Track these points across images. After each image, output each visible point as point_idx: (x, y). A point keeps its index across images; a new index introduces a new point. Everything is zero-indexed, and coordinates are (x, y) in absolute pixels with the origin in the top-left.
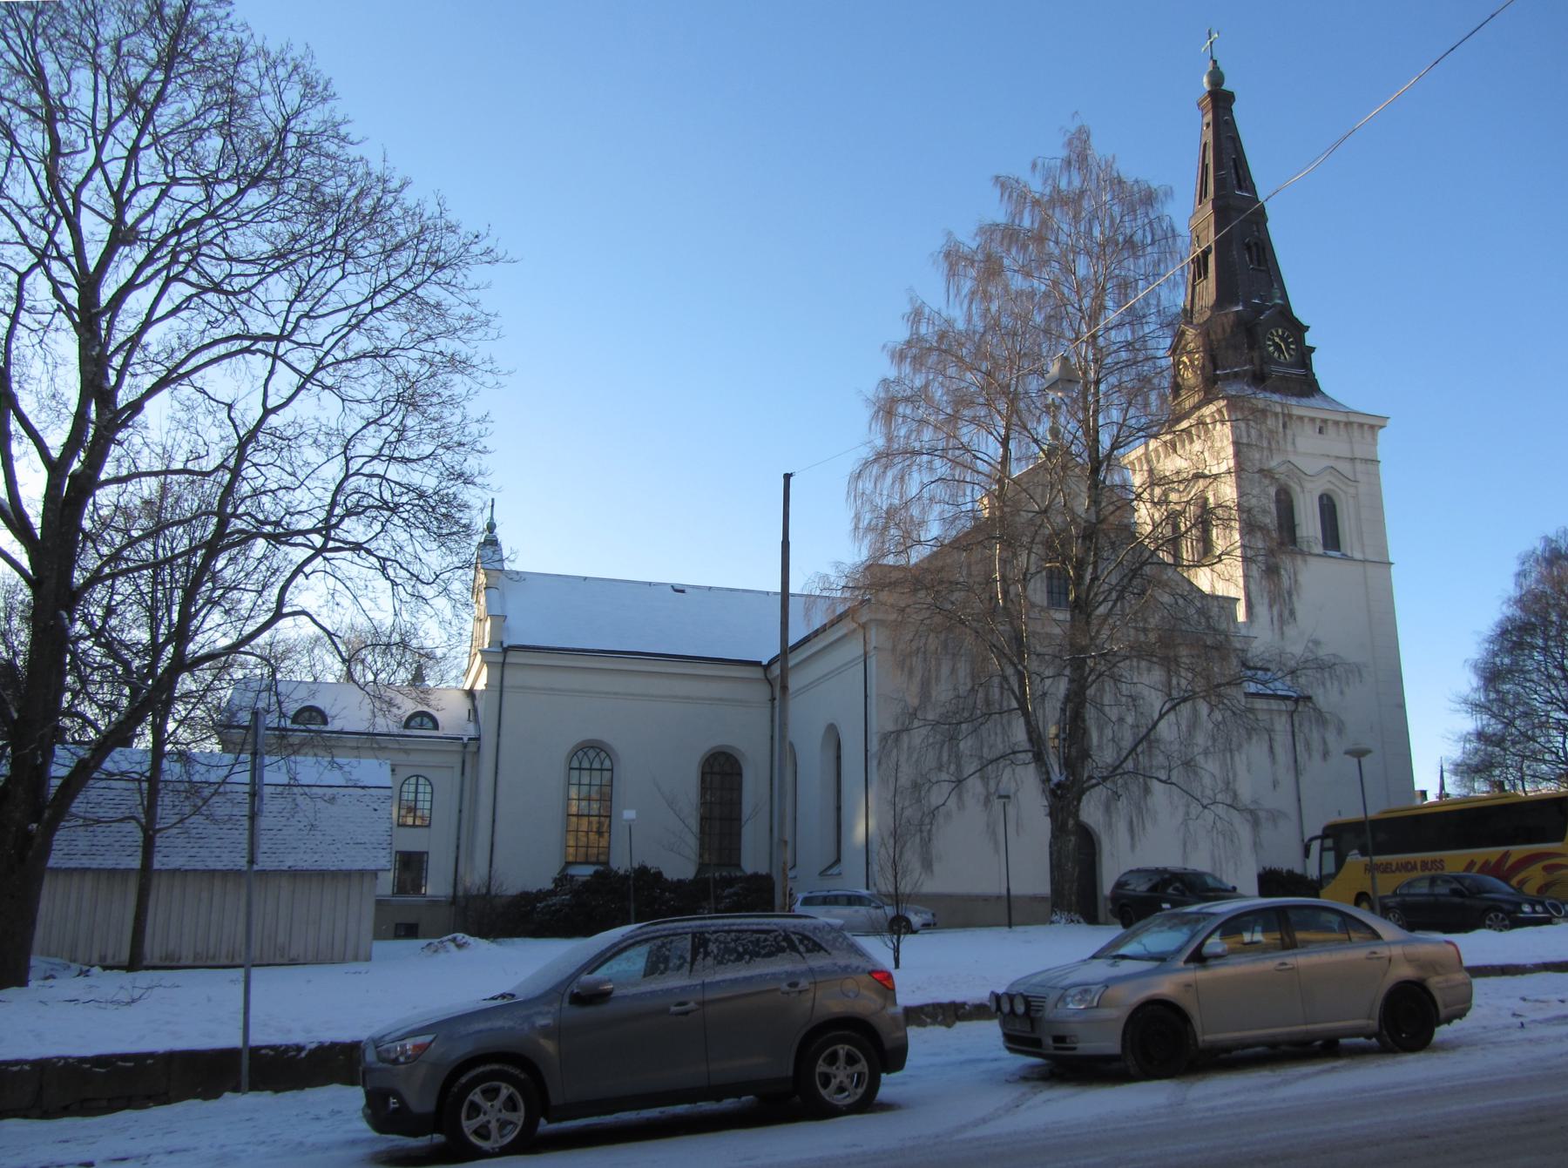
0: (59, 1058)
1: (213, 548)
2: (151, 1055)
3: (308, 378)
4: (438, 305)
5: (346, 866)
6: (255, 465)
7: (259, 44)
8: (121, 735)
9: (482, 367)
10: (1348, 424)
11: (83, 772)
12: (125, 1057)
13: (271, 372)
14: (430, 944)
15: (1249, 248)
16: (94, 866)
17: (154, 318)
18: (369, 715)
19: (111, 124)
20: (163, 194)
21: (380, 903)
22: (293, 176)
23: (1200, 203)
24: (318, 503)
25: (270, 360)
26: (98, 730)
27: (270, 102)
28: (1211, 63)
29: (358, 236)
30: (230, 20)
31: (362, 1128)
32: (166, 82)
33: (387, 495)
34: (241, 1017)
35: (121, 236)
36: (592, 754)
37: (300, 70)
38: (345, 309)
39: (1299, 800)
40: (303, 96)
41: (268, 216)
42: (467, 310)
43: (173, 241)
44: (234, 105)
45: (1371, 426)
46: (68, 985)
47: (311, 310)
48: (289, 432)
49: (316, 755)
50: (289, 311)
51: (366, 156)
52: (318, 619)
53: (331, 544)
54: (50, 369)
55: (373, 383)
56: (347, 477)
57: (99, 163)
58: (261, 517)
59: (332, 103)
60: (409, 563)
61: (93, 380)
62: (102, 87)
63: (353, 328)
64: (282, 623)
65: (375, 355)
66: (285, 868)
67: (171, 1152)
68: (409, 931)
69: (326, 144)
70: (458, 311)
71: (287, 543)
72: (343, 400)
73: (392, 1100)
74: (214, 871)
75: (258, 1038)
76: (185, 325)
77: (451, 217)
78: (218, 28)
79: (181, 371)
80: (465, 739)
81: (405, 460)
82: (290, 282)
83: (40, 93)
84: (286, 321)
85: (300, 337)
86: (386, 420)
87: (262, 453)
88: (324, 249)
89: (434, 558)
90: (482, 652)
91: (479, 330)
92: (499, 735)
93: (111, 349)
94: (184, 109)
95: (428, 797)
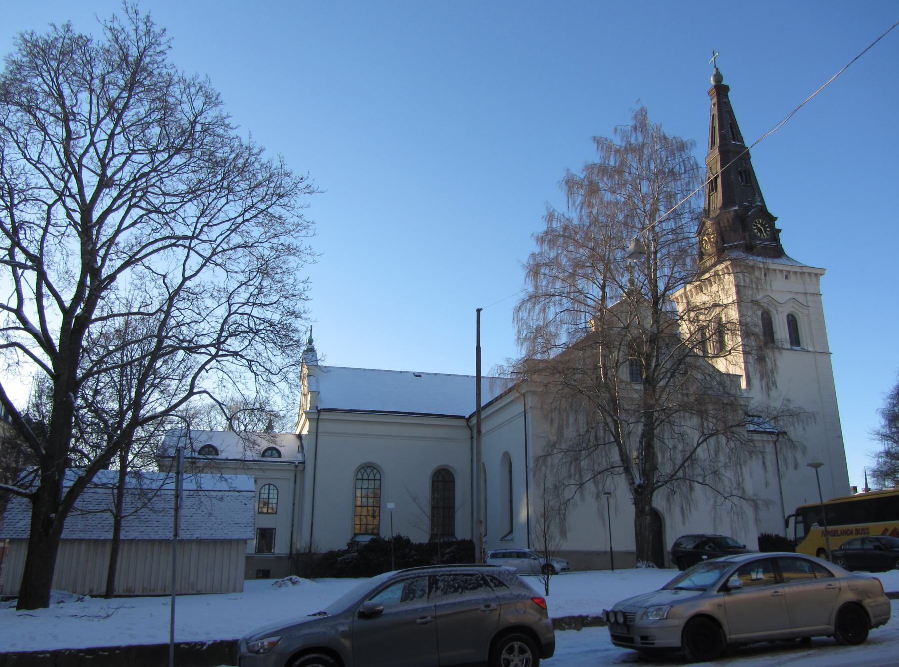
0: (67, 650)
3: (208, 260)
4: (280, 218)
5: (229, 536)
6: (178, 309)
7: (180, 75)
8: (102, 463)
9: (305, 251)
10: (802, 273)
11: (81, 484)
12: (103, 649)
13: (187, 257)
14: (277, 582)
15: (740, 173)
16: (87, 538)
18: (242, 450)
19: (99, 122)
20: (128, 159)
21: (248, 558)
22: (199, 147)
23: (711, 149)
24: (213, 330)
25: (186, 250)
27: (186, 107)
28: (715, 70)
29: (236, 180)
30: (164, 63)
32: (130, 97)
33: (252, 325)
35: (105, 183)
36: (369, 471)
37: (203, 89)
39: (781, 493)
40: (204, 104)
41: (185, 170)
42: (296, 220)
43: (133, 185)
45: (816, 274)
46: (72, 607)
47: (210, 221)
48: (197, 290)
49: (212, 473)
50: (197, 222)
52: (213, 395)
53: (221, 353)
55: (244, 261)
56: (229, 315)
57: (92, 143)
58: (181, 338)
59: (220, 107)
60: (264, 363)
63: (233, 231)
65: (245, 246)
66: (195, 538)
68: (264, 574)
70: (291, 221)
71: (196, 353)
72: (227, 272)
74: (154, 540)
75: (179, 638)
76: (140, 232)
77: (287, 168)
78: (158, 68)
79: (137, 257)
80: (297, 463)
81: (262, 305)
82: (197, 206)
83: (61, 106)
84: (195, 228)
85: (203, 237)
86: (251, 282)
88: (217, 188)
89: (279, 360)
91: (303, 231)
92: (315, 460)
93: (99, 245)
94: (139, 112)
95: (275, 496)
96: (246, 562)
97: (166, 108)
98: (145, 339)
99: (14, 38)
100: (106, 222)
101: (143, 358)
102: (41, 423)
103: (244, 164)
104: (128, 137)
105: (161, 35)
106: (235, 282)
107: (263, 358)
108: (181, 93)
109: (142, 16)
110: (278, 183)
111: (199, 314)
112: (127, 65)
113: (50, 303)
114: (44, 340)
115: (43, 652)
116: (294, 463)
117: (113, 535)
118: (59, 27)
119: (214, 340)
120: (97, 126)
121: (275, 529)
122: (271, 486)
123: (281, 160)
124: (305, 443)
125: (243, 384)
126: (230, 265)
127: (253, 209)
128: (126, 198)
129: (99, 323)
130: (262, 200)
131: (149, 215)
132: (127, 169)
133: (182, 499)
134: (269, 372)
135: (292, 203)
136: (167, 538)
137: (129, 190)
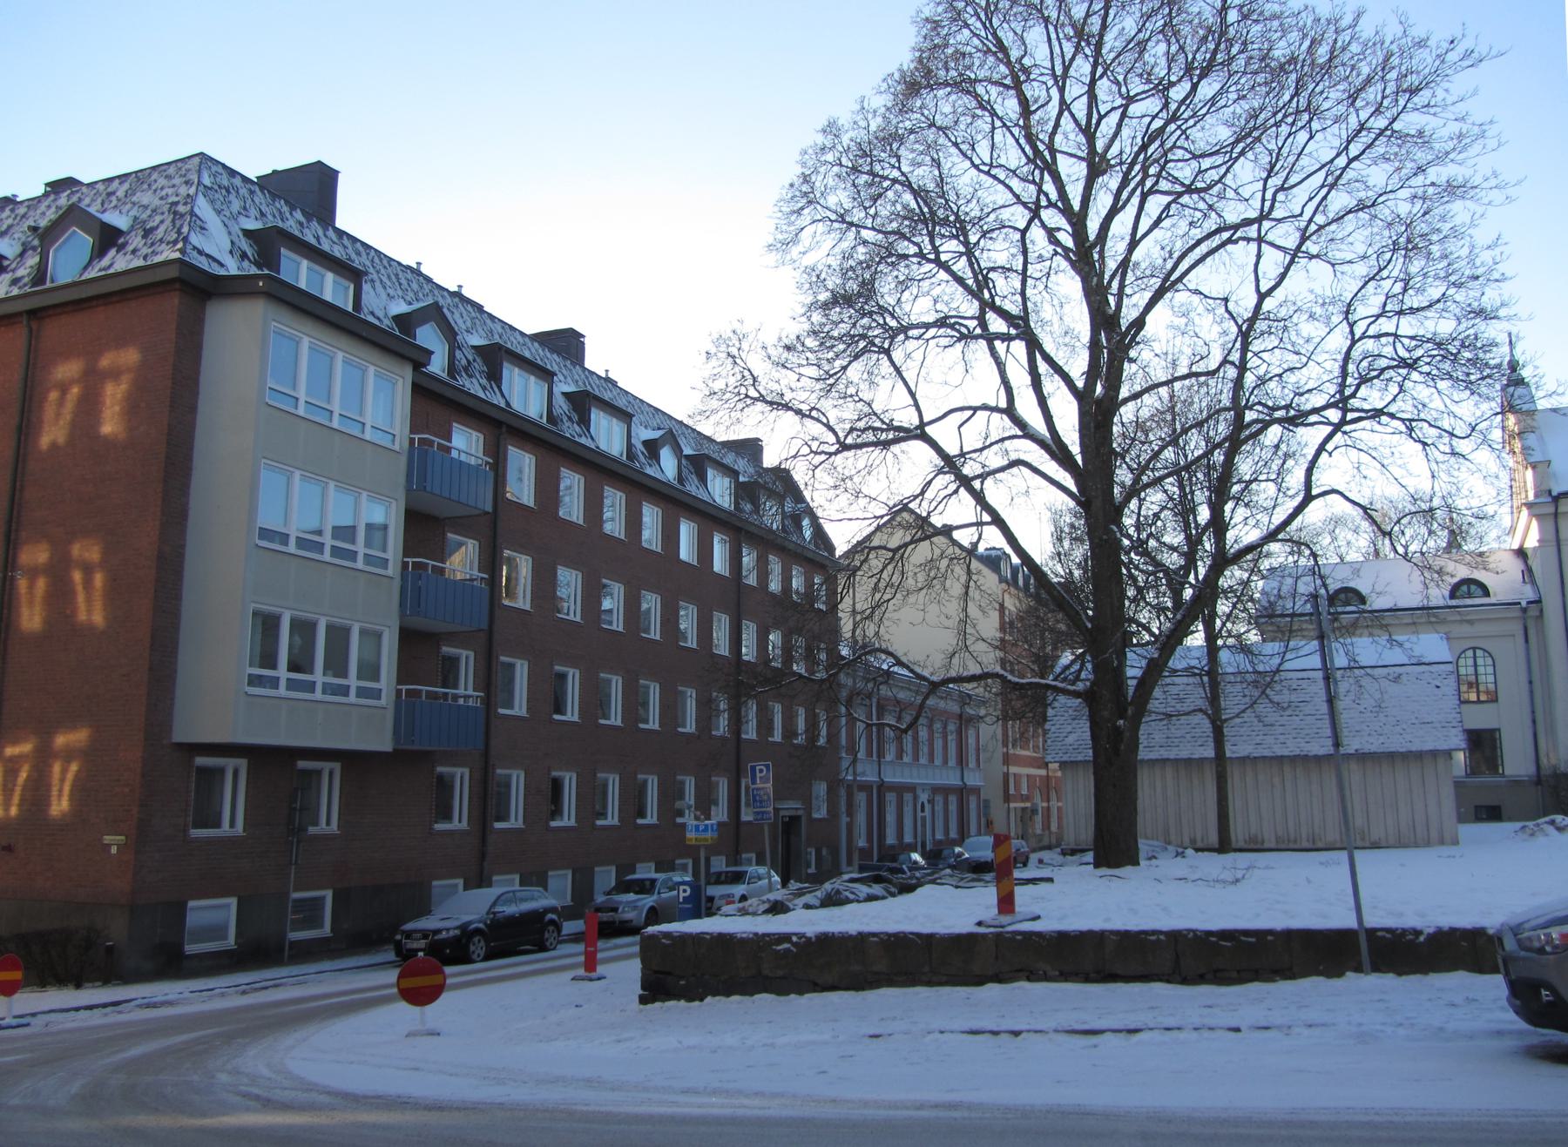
0: (1189, 931)
1: (1234, 443)
3: (1295, 254)
4: (1421, 133)
6: (1256, 354)
8: (1171, 640)
9: (1485, 185)
11: (1155, 670)
12: (1247, 933)
13: (1259, 256)
16: (1172, 757)
17: (1138, 238)
18: (1421, 587)
19: (1066, 69)
20: (1124, 116)
21: (1458, 785)
24: (1325, 378)
25: (1253, 246)
26: (1151, 634)
31: (1510, 1019)
33: (1403, 353)
35: (1096, 166)
41: (1222, 102)
42: (1454, 128)
46: (1169, 866)
47: (1285, 182)
48: (1283, 313)
49: (1371, 635)
52: (1347, 494)
53: (1350, 416)
55: (1362, 239)
56: (1354, 342)
57: (1064, 106)
58: (1270, 404)
60: (1435, 420)
63: (1332, 186)
64: (1314, 505)
65: (1361, 207)
66: (1352, 752)
67: (1310, 1026)
68: (1491, 814)
70: (1445, 133)
72: (1333, 265)
73: (1544, 992)
75: (1373, 920)
76: (1169, 234)
77: (1418, 32)
80: (1524, 604)
81: (1413, 311)
84: (1263, 200)
85: (1277, 214)
86: (1385, 273)
87: (1261, 340)
88: (1285, 116)
89: (1468, 408)
90: (1529, 506)
91: (1475, 145)
93: (1107, 277)
95: (1490, 670)
98: (1209, 417)
100: (1110, 234)
101: (1208, 453)
103: (1332, 53)
106: (1352, 281)
107: (1433, 412)
113: (1053, 386)
114: (1057, 450)
115: (1154, 932)
121: (1499, 730)
123: (1403, 19)
128: (1132, 185)
129: (1131, 406)
130: (1378, 111)
133: (1336, 682)
134: (1452, 435)
135: (1439, 99)
137: (1137, 167)
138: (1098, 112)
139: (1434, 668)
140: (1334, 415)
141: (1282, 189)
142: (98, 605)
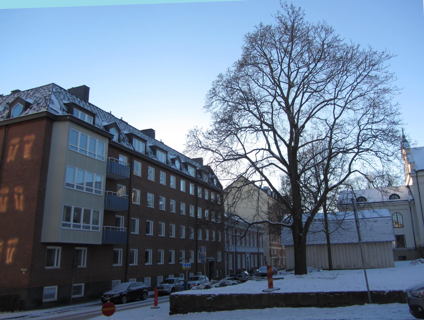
0: (321, 292)
1: (330, 157)
2: (343, 292)
3: (344, 108)
4: (376, 76)
5: (382, 240)
6: (335, 134)
7: (312, 25)
9: (393, 89)
11: (310, 220)
13: (334, 108)
14: (412, 262)
16: (315, 244)
18: (381, 196)
19: (282, 60)
21: (394, 250)
22: (328, 56)
24: (353, 140)
25: (333, 106)
27: (318, 39)
29: (349, 65)
30: (304, 23)
32: (292, 44)
33: (373, 134)
34: (365, 283)
35: (291, 85)
37: (324, 27)
38: (350, 86)
40: (326, 35)
41: (324, 68)
42: (385, 75)
43: (303, 83)
44: (310, 43)
46: (316, 274)
47: (341, 89)
48: (341, 123)
49: (368, 209)
50: (335, 91)
51: (345, 43)
52: (360, 171)
53: (360, 151)
54: (281, 123)
55: (362, 104)
57: (282, 70)
59: (333, 33)
60: (383, 151)
61: (292, 123)
62: (279, 52)
63: (353, 90)
65: (361, 95)
66: (365, 242)
68: (403, 258)
69: (334, 44)
70: (382, 76)
71: (348, 153)
72: (354, 111)
73: (419, 309)
74: (346, 243)
75: (371, 289)
76: (310, 103)
77: (374, 50)
78: (301, 26)
79: (312, 114)
80: (409, 200)
81: (376, 122)
82: (333, 83)
83: (266, 59)
84: (335, 94)
85: (339, 97)
86: (368, 113)
87: (336, 131)
88: (340, 72)
89: (392, 148)
90: (410, 174)
91: (390, 79)
92: (420, 198)
94: (297, 50)
95: (401, 219)
96: (393, 253)
97: (309, 43)
99: (243, 38)
101: (323, 161)
102: (286, 196)
103: (352, 56)
104: (295, 62)
105: (299, 11)
107: (382, 149)
108: (314, 33)
109: (289, 6)
110: (371, 59)
111: (346, 134)
112: (288, 31)
113: (280, 143)
116: (408, 200)
117: (327, 242)
118: (258, 26)
119: (355, 145)
120: (282, 62)
121: (404, 235)
122: (398, 213)
123: (370, 47)
124: (412, 190)
125: (374, 164)
126: (355, 107)
127: (361, 76)
128: (300, 90)
130: (364, 70)
131: (313, 94)
132: (298, 76)
136: (352, 242)
137: (302, 86)
138: (291, 71)
139: (386, 218)
140: (356, 150)
141: (340, 91)
142: (21, 204)
